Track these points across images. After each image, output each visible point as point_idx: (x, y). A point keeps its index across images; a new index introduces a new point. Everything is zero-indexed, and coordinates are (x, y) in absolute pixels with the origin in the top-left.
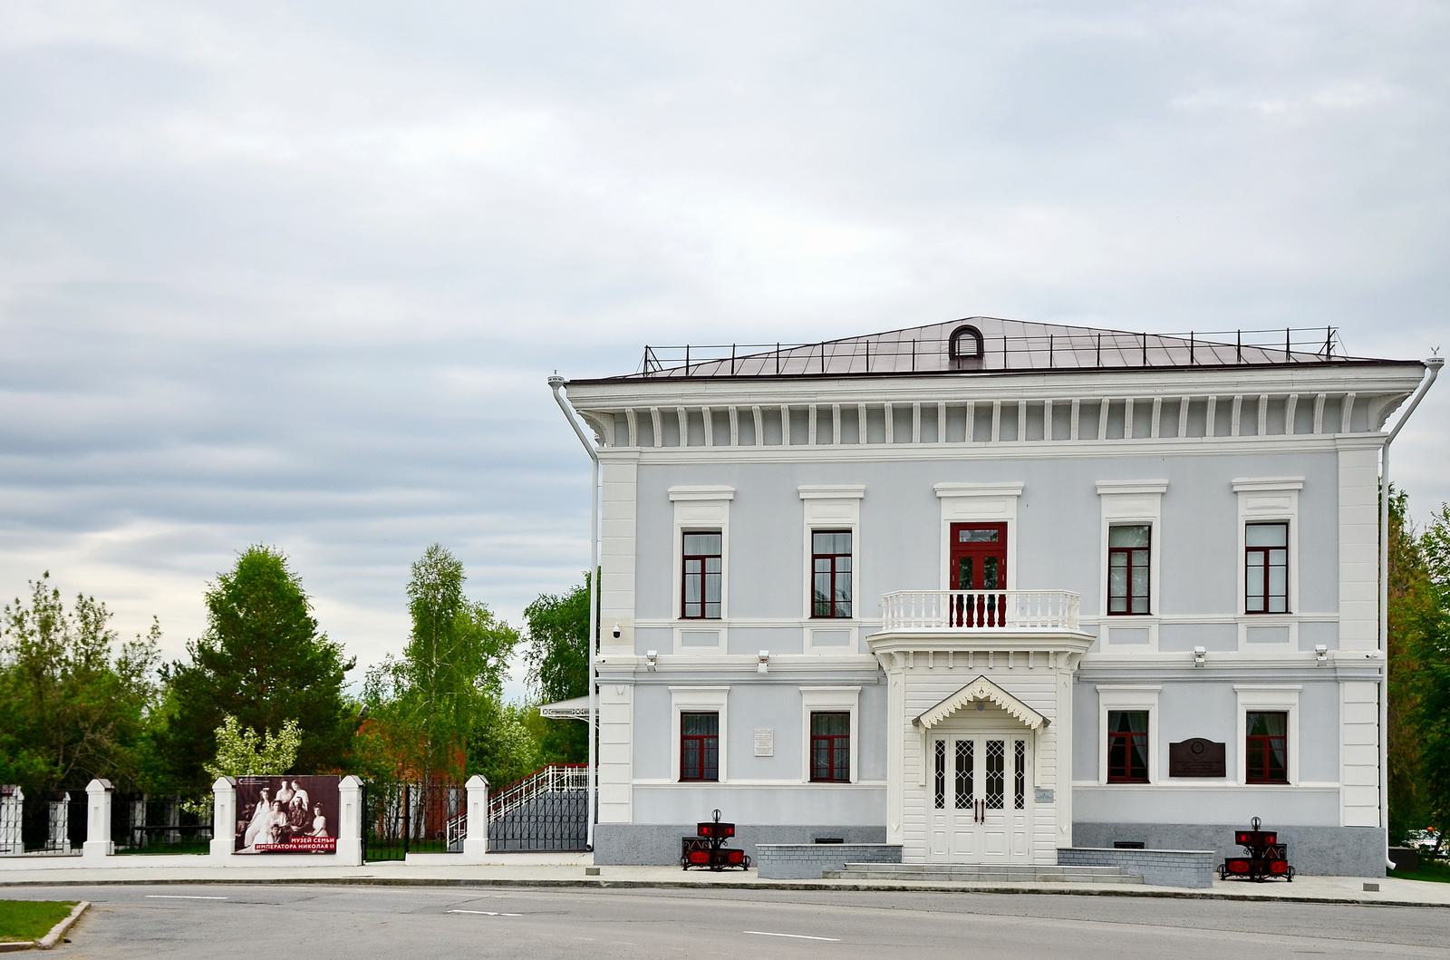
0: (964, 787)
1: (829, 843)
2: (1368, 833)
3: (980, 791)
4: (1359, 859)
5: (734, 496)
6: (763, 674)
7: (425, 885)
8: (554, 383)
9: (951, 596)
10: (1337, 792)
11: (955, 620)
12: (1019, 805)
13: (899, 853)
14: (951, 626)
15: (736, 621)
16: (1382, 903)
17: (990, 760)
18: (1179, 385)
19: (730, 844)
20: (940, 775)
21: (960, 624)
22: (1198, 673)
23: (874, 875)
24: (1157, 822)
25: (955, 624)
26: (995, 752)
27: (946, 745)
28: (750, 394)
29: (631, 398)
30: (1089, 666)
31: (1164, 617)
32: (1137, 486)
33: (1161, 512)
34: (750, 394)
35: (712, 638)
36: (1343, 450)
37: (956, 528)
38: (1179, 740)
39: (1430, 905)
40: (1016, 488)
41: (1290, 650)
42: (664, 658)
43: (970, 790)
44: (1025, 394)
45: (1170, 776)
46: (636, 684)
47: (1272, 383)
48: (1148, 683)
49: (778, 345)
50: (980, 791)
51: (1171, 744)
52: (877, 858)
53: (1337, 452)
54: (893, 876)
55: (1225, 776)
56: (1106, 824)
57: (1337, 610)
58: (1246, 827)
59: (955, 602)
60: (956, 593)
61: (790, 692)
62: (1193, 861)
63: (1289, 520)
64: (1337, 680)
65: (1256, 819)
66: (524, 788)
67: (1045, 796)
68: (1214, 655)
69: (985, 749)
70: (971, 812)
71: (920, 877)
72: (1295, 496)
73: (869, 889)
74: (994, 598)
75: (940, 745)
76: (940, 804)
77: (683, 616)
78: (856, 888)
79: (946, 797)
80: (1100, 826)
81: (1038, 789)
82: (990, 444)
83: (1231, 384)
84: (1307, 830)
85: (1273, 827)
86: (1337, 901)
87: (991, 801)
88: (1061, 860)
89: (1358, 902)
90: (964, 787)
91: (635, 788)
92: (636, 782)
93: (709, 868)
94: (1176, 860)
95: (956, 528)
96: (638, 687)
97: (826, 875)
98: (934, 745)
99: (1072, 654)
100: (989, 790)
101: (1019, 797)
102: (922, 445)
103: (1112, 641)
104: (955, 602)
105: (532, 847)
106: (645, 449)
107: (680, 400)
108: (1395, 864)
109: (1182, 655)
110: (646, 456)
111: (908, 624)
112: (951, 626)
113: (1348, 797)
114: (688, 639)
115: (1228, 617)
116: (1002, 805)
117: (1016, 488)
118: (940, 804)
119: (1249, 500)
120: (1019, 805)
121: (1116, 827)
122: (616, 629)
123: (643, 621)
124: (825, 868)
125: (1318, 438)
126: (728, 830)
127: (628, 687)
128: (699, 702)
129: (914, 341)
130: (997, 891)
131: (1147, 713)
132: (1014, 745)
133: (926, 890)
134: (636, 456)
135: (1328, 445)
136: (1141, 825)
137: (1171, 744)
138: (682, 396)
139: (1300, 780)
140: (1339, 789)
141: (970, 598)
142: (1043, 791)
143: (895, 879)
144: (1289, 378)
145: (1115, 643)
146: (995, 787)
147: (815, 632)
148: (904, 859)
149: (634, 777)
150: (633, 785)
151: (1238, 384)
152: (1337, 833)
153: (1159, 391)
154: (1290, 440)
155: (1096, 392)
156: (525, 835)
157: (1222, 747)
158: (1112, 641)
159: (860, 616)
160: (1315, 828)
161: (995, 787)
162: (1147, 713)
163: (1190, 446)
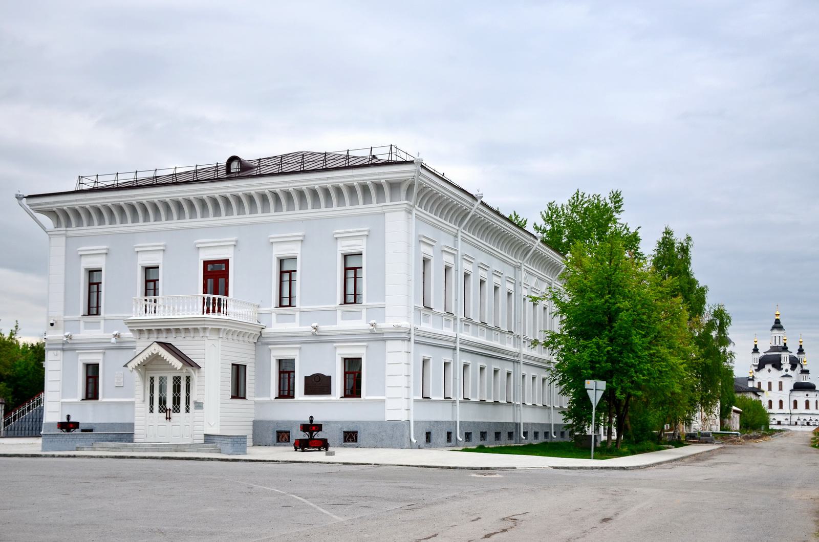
0: (163, 402)
1: (87, 432)
2: (397, 424)
3: (169, 404)
4: (392, 439)
5: (304, 238)
6: (113, 343)
7: (620, 469)
8: (19, 198)
9: (204, 298)
10: (383, 402)
11: (205, 311)
12: (187, 411)
13: (132, 437)
14: (203, 314)
15: (108, 316)
16: (290, 462)
17: (174, 386)
18: (312, 180)
19: (319, 435)
20: (188, 394)
21: (208, 312)
22: (317, 338)
23: (99, 449)
24: (336, 420)
25: (205, 313)
26: (177, 383)
27: (155, 379)
28: (105, 198)
29: (54, 203)
30: (266, 335)
31: (302, 307)
32: (94, 250)
33: (301, 250)
34: (105, 198)
35: (357, 315)
36: (389, 212)
37: (206, 263)
38: (309, 375)
39: (312, 462)
40: (232, 241)
41: (360, 324)
42: (76, 336)
43: (165, 403)
44: (229, 190)
45: (305, 394)
46: (63, 350)
47: (344, 177)
48: (282, 344)
49: (197, 166)
50: (169, 404)
51: (305, 377)
52: (115, 440)
53: (384, 213)
54: (108, 449)
55: (330, 393)
56: (273, 421)
57: (385, 301)
58: (305, 420)
59: (206, 301)
60: (206, 296)
61: (329, 346)
62: (230, 440)
63: (86, 269)
64: (384, 340)
65: (311, 417)
66: (31, 404)
67: (199, 406)
68: (324, 328)
69: (172, 381)
70: (164, 415)
71: (119, 450)
72: (299, 244)
73: (59, 456)
74: (215, 301)
75: (152, 379)
76: (151, 411)
77: (345, 303)
78: (53, 456)
79: (154, 407)
80: (269, 422)
81: (196, 402)
82: (320, 210)
83: (324, 179)
84: (368, 423)
85: (321, 421)
86: (357, 464)
87: (174, 409)
88: (206, 440)
89: (279, 462)
90: (163, 402)
91: (62, 403)
92: (256, 399)
93: (317, 449)
94: (50, 437)
95: (206, 263)
96: (65, 352)
97: (77, 449)
98: (149, 379)
99: (235, 331)
100: (174, 403)
101: (152, 407)
102: (190, 220)
103: (278, 322)
104: (206, 301)
105: (30, 435)
106: (68, 229)
107: (75, 203)
108: (415, 441)
109: (308, 328)
110: (69, 232)
111: (193, 314)
112: (203, 314)
113: (389, 404)
114: (88, 326)
115: (332, 306)
116: (179, 411)
117: (365, 231)
118: (151, 411)
119: (342, 242)
120: (187, 411)
121: (277, 423)
122: (52, 322)
123: (67, 317)
124: (78, 445)
125: (374, 206)
126: (319, 427)
127: (59, 352)
128: (92, 359)
129: (176, 168)
130: (116, 457)
131: (294, 360)
132: (185, 378)
133: (85, 456)
134: (64, 232)
135: (379, 210)
136: (289, 422)
137: (305, 377)
138: (76, 200)
139: (367, 395)
140: (385, 400)
141: (214, 299)
142: (198, 403)
143: (108, 451)
144: (351, 174)
145: (279, 323)
146: (176, 401)
147: (86, 322)
148: (136, 440)
149: (62, 398)
150: (62, 402)
151: (328, 178)
152: (382, 424)
153: (291, 185)
154: (361, 208)
155: (262, 187)
156: (30, 428)
157: (330, 377)
158: (278, 322)
159: (367, 302)
160: (372, 422)
161: (176, 401)
162: (294, 360)
163: (343, 211)
